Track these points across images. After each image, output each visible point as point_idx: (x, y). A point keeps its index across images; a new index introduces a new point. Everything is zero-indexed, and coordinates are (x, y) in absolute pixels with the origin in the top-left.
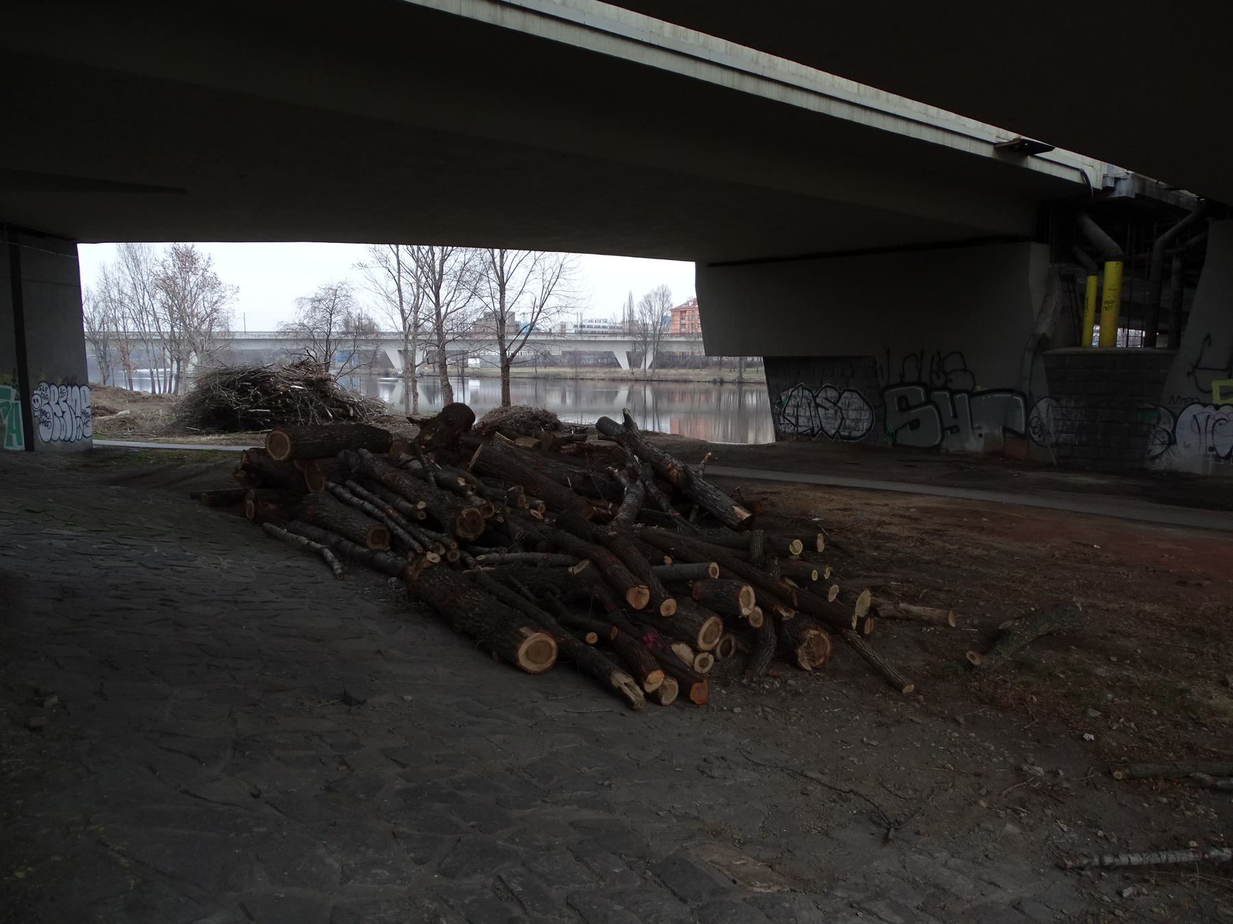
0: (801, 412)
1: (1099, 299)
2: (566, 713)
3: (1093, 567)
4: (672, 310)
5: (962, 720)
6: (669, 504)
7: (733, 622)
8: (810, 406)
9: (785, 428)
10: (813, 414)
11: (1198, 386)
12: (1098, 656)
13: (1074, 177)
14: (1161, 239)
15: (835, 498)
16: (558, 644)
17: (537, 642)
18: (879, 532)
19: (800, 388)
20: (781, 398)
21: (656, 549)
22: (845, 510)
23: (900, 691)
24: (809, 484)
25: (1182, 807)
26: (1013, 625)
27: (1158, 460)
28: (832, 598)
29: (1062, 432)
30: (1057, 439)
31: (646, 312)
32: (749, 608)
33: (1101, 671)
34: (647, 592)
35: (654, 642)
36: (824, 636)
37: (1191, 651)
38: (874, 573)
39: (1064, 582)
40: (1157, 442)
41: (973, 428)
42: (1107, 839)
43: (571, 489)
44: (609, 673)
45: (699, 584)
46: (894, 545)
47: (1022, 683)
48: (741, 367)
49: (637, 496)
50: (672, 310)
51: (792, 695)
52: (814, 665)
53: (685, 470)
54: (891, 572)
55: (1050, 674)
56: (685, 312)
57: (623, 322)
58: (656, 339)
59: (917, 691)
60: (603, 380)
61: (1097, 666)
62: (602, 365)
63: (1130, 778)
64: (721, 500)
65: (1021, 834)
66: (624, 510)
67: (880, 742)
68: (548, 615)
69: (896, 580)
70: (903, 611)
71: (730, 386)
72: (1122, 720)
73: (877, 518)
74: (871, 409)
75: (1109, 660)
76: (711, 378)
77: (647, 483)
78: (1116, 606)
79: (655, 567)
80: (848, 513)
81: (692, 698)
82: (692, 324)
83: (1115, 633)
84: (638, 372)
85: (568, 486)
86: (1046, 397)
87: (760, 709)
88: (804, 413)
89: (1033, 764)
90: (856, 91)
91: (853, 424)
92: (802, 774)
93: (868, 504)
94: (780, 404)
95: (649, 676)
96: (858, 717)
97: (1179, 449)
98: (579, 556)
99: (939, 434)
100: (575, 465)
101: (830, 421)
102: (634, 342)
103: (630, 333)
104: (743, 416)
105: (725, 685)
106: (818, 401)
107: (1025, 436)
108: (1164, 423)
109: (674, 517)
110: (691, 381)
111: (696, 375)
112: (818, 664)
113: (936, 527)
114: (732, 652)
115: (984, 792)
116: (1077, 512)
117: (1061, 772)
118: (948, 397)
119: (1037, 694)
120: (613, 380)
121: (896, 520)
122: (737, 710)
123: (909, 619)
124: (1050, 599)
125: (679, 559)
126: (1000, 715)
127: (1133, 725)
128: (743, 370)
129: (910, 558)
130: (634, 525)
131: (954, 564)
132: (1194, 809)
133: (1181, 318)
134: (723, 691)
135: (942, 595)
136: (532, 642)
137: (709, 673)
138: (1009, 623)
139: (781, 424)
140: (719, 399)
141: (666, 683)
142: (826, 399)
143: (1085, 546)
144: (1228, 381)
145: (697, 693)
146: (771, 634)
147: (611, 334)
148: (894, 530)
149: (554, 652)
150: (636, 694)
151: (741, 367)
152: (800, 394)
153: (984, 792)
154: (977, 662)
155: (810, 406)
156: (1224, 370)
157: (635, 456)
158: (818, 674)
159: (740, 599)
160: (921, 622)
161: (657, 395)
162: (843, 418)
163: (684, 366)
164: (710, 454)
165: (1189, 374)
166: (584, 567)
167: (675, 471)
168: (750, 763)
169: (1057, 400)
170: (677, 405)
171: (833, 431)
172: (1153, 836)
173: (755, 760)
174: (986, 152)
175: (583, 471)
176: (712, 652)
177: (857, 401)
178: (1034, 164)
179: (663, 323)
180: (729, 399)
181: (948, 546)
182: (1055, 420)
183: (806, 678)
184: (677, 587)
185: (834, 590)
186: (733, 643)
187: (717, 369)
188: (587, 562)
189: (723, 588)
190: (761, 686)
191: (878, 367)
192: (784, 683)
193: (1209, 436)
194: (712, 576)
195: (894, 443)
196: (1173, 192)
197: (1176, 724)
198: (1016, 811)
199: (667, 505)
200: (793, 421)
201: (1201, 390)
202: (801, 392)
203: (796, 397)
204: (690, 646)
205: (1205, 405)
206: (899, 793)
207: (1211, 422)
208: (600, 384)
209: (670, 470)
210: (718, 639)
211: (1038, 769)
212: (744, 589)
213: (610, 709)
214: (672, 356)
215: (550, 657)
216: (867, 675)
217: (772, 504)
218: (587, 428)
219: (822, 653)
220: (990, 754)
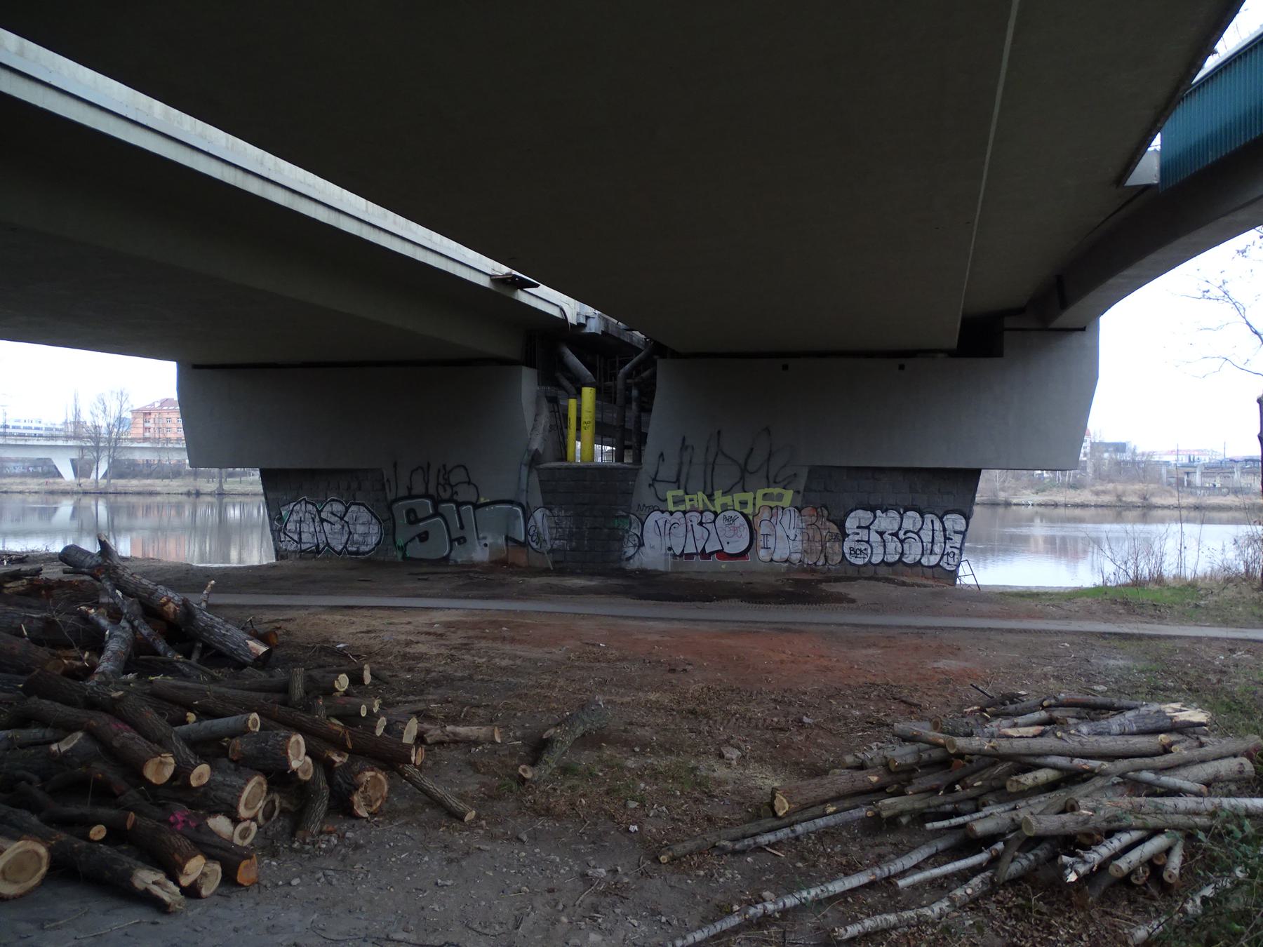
0: (305, 527)
1: (579, 419)
2: (77, 941)
3: (603, 665)
4: (132, 412)
5: (525, 838)
6: (167, 645)
7: (279, 778)
8: (314, 521)
10: (318, 529)
11: (657, 496)
12: (625, 749)
13: (555, 312)
14: (622, 371)
15: (355, 619)
16: (50, 850)
17: (18, 854)
18: (409, 653)
19: (303, 502)
20: (281, 514)
21: (174, 706)
22: (368, 632)
23: (462, 820)
24: (323, 606)
25: (716, 875)
26: (555, 732)
27: (632, 561)
28: (379, 732)
29: (556, 539)
30: (552, 546)
31: (99, 412)
32: (299, 760)
33: (631, 763)
34: (172, 760)
35: (184, 821)
36: (381, 776)
37: (691, 731)
38: (411, 698)
39: (583, 682)
40: (630, 544)
41: (478, 538)
42: (669, 923)
43: (27, 639)
44: (129, 874)
45: (236, 741)
46: (426, 664)
47: (570, 788)
48: (221, 478)
49: (124, 640)
50: (132, 412)
51: (353, 850)
52: (372, 810)
53: (185, 604)
54: (429, 694)
55: (591, 774)
56: (150, 414)
57: (66, 423)
58: (113, 444)
59: (478, 817)
60: (36, 493)
61: (627, 759)
62: (35, 475)
63: (673, 859)
64: (232, 635)
65: (603, 940)
66: (108, 660)
67: (454, 880)
68: (26, 814)
69: (434, 701)
70: (451, 735)
71: (209, 499)
72: (655, 806)
73: (403, 637)
75: (634, 750)
76: (184, 490)
77: (136, 623)
78: (628, 699)
79: (176, 729)
80: (373, 635)
81: (239, 880)
82: (159, 428)
83: (632, 724)
84: (87, 483)
85: (22, 636)
87: (321, 874)
88: (308, 528)
89: (595, 867)
90: (364, 209)
91: (361, 539)
92: (388, 939)
93: (391, 624)
94: (280, 519)
95: (187, 866)
96: (426, 859)
97: (646, 550)
98: (67, 728)
100: (30, 607)
101: (336, 536)
102: (82, 448)
103: (76, 437)
104: (225, 532)
105: (274, 854)
106: (323, 515)
107: (525, 544)
108: (635, 528)
109: (178, 661)
110: (158, 494)
111: (165, 486)
112: (374, 808)
113: (460, 641)
114: (276, 813)
115: (560, 907)
116: (580, 614)
117: (619, 868)
119: (584, 796)
120: (52, 493)
121: (422, 638)
122: (295, 882)
123: (456, 741)
125: (206, 713)
126: (557, 825)
127: (664, 808)
128: (223, 480)
129: (443, 676)
130: (123, 677)
131: (486, 678)
132: (723, 875)
133: (642, 439)
134: (274, 863)
135: (481, 712)
136: (12, 855)
137: (252, 844)
138: (552, 731)
140: (194, 514)
141: (206, 870)
142: (332, 513)
143: (594, 645)
145: (245, 873)
146: (323, 784)
147: (46, 437)
148: (421, 648)
149: (45, 861)
150: (169, 893)
151: (221, 478)
152: (303, 508)
153: (560, 907)
154: (528, 775)
155: (314, 521)
156: (674, 482)
157: (117, 591)
158: (376, 819)
159: (289, 751)
160: (470, 743)
161: (113, 510)
163: (148, 476)
164: (213, 582)
165: (650, 485)
166: (76, 741)
167: (171, 605)
168: (329, 941)
169: (550, 510)
170: (140, 521)
171: (340, 547)
172: (701, 909)
173: (333, 937)
174: (484, 282)
175: (45, 614)
176: (254, 819)
177: (365, 515)
178: (522, 297)
179: (122, 425)
180: (207, 513)
181: (478, 660)
182: (550, 528)
183: (364, 827)
184: (208, 748)
185: (382, 722)
186: (277, 804)
187: (192, 480)
188: (80, 735)
189: (267, 742)
190: (317, 846)
191: (385, 480)
192: (342, 838)
193: (667, 537)
194: (252, 729)
195: (404, 557)
196: (629, 332)
197: (696, 800)
198: (594, 919)
199: (165, 647)
200: (296, 537)
201: (660, 500)
202: (304, 506)
203: (299, 513)
204: (229, 817)
205: (663, 512)
206: (486, 931)
207: (668, 526)
208: (31, 498)
209: (164, 604)
210: (261, 802)
211: (600, 870)
212: (293, 739)
213: (137, 921)
214: (133, 464)
215: (39, 869)
216: (427, 810)
217: (288, 633)
218: (27, 556)
219: (379, 795)
220: (557, 866)
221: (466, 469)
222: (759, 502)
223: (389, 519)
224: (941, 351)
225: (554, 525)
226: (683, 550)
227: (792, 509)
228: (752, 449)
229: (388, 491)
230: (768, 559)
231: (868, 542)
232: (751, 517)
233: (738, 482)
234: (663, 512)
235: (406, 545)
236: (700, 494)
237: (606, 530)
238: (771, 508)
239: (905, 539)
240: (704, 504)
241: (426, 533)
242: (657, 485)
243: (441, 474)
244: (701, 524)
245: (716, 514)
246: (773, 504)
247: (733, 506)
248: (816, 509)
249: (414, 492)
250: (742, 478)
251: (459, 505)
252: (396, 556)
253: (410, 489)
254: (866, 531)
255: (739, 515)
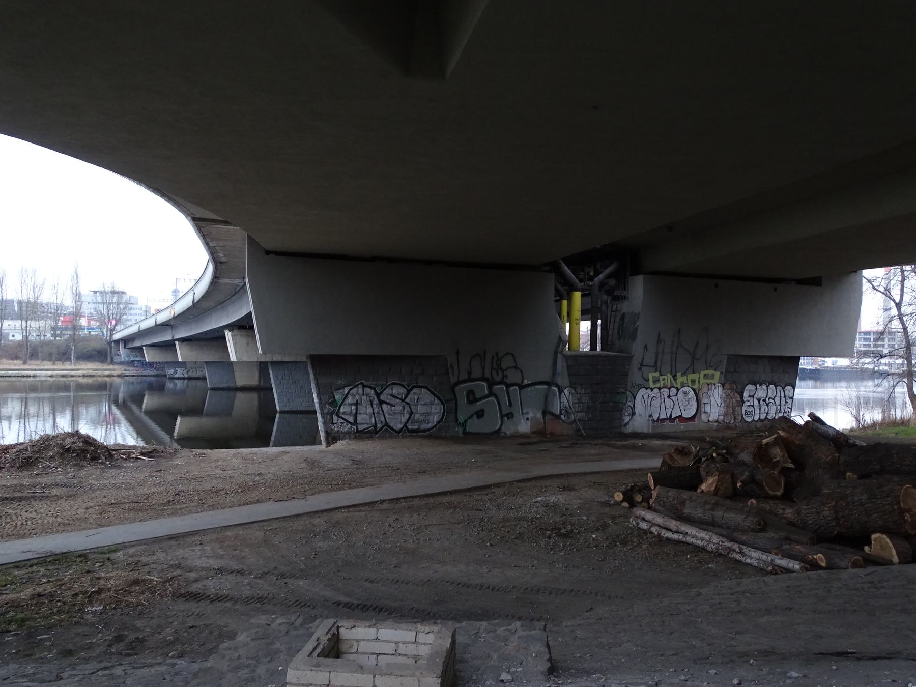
8: (372, 404)
9: (338, 427)
29: (578, 412)
41: (523, 414)
74: (442, 403)
86: (567, 387)
91: (422, 418)
94: (333, 403)
97: (636, 417)
99: (499, 421)
106: (382, 397)
108: (629, 401)
118: (505, 389)
124: (50, 531)
139: (333, 424)
142: (392, 395)
144: (655, 373)
155: (372, 404)
162: (411, 413)
169: (575, 389)
177: (426, 396)
191: (449, 365)
195: (464, 432)
200: (351, 419)
207: (650, 399)
221: (514, 357)
222: (702, 381)
223: (452, 399)
224: (793, 280)
225: (577, 401)
226: (659, 416)
227: (719, 384)
228: (698, 343)
229: (451, 375)
230: (707, 421)
231: (753, 406)
232: (697, 391)
233: (690, 367)
234: (647, 389)
235: (466, 421)
236: (669, 375)
237: (611, 404)
238: (708, 385)
239: (769, 403)
240: (671, 383)
241: (483, 410)
242: (644, 369)
243: (494, 361)
244: (669, 397)
245: (678, 390)
246: (709, 381)
247: (688, 383)
248: (731, 384)
249: (473, 376)
250: (692, 363)
251: (508, 386)
252: (457, 431)
253: (470, 373)
254: (752, 398)
255: (691, 390)
